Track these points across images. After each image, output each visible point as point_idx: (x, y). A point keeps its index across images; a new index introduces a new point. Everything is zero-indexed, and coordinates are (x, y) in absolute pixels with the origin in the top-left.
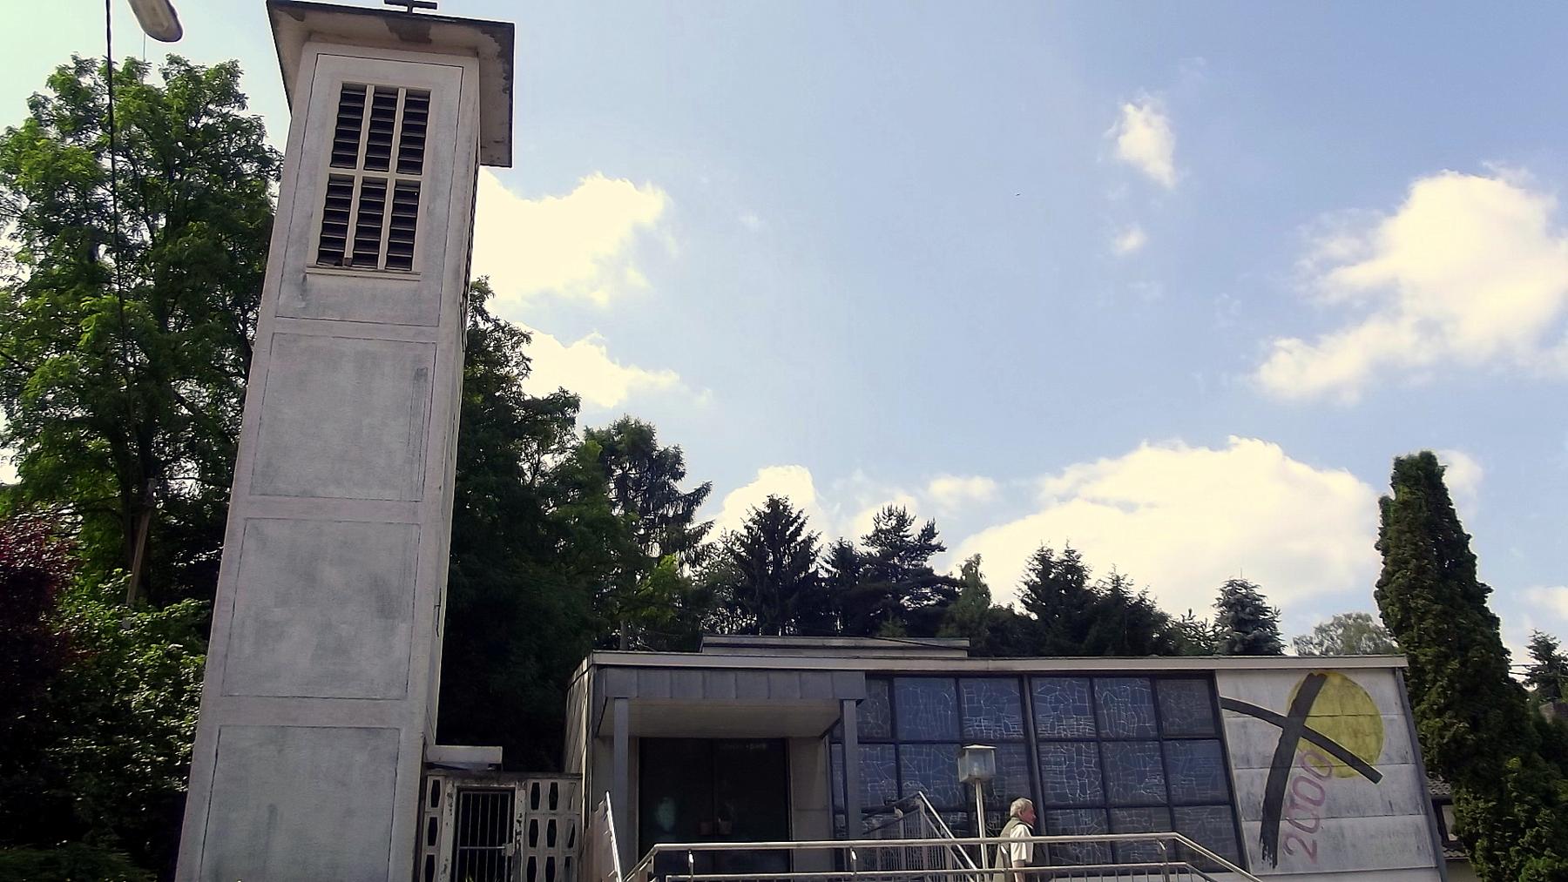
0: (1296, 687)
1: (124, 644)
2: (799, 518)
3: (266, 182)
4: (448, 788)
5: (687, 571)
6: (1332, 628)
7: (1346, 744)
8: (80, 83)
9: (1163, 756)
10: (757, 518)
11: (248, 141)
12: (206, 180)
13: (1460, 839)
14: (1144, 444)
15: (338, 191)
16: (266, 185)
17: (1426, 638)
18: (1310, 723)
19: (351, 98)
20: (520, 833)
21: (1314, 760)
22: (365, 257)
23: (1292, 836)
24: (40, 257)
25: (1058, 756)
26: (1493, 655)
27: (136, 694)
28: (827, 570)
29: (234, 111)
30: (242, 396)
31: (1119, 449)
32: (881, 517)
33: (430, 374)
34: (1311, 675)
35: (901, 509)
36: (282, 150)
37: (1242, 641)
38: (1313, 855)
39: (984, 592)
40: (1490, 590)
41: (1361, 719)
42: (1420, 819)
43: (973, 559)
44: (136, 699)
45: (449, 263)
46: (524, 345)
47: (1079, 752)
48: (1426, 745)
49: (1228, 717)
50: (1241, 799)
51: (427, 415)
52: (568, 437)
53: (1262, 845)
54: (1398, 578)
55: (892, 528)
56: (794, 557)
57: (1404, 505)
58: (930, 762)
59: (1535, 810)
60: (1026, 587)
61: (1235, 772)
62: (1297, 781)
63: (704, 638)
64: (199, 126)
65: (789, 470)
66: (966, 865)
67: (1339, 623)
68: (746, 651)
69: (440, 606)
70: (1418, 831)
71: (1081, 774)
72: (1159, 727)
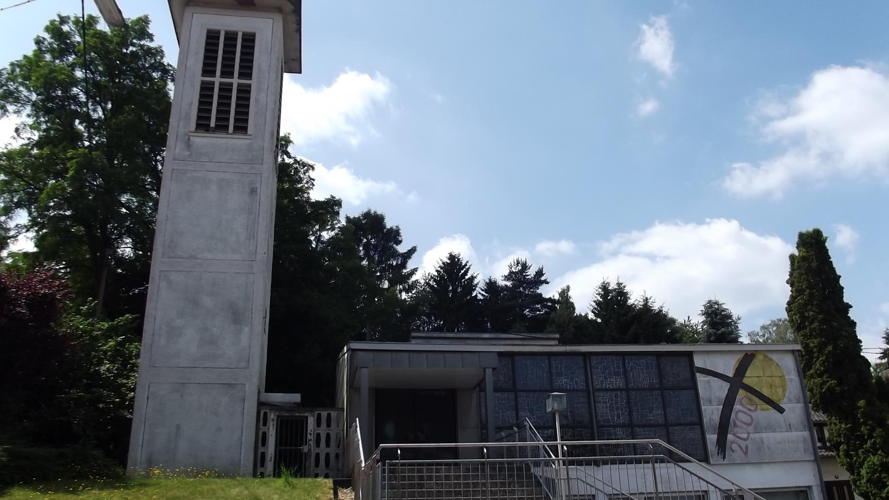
0: (738, 360)
1: (95, 339)
2: (467, 265)
3: (166, 82)
4: (272, 416)
5: (404, 296)
6: (770, 327)
7: (766, 392)
8: (62, 29)
9: (663, 399)
10: (442, 265)
11: (155, 60)
12: (132, 82)
13: (831, 445)
14: (657, 222)
15: (206, 90)
16: (166, 84)
17: (814, 333)
18: (746, 381)
19: (212, 37)
20: (310, 440)
21: (747, 401)
22: (222, 127)
23: (733, 443)
24: (44, 126)
25: (605, 399)
26: (851, 343)
27: (102, 366)
28: (482, 295)
29: (146, 42)
30: (156, 202)
31: (644, 225)
32: (512, 265)
33: (259, 190)
34: (746, 354)
35: (523, 260)
36: (175, 65)
37: (715, 334)
38: (746, 453)
39: (571, 307)
40: (851, 307)
41: (774, 379)
42: (806, 434)
43: (565, 288)
44: (103, 368)
45: (268, 129)
46: (311, 171)
47: (616, 396)
48: (813, 393)
49: (701, 378)
50: (706, 422)
51: (257, 213)
52: (336, 221)
53: (717, 447)
54: (799, 300)
55: (519, 271)
56: (463, 287)
57: (803, 259)
58: (534, 401)
59: (872, 430)
60: (595, 304)
61: (703, 408)
62: (737, 412)
63: (412, 334)
64: (128, 52)
65: (465, 237)
66: (550, 456)
67: (774, 324)
68: (434, 341)
69: (266, 317)
70: (805, 440)
71: (617, 408)
72: (661, 382)
